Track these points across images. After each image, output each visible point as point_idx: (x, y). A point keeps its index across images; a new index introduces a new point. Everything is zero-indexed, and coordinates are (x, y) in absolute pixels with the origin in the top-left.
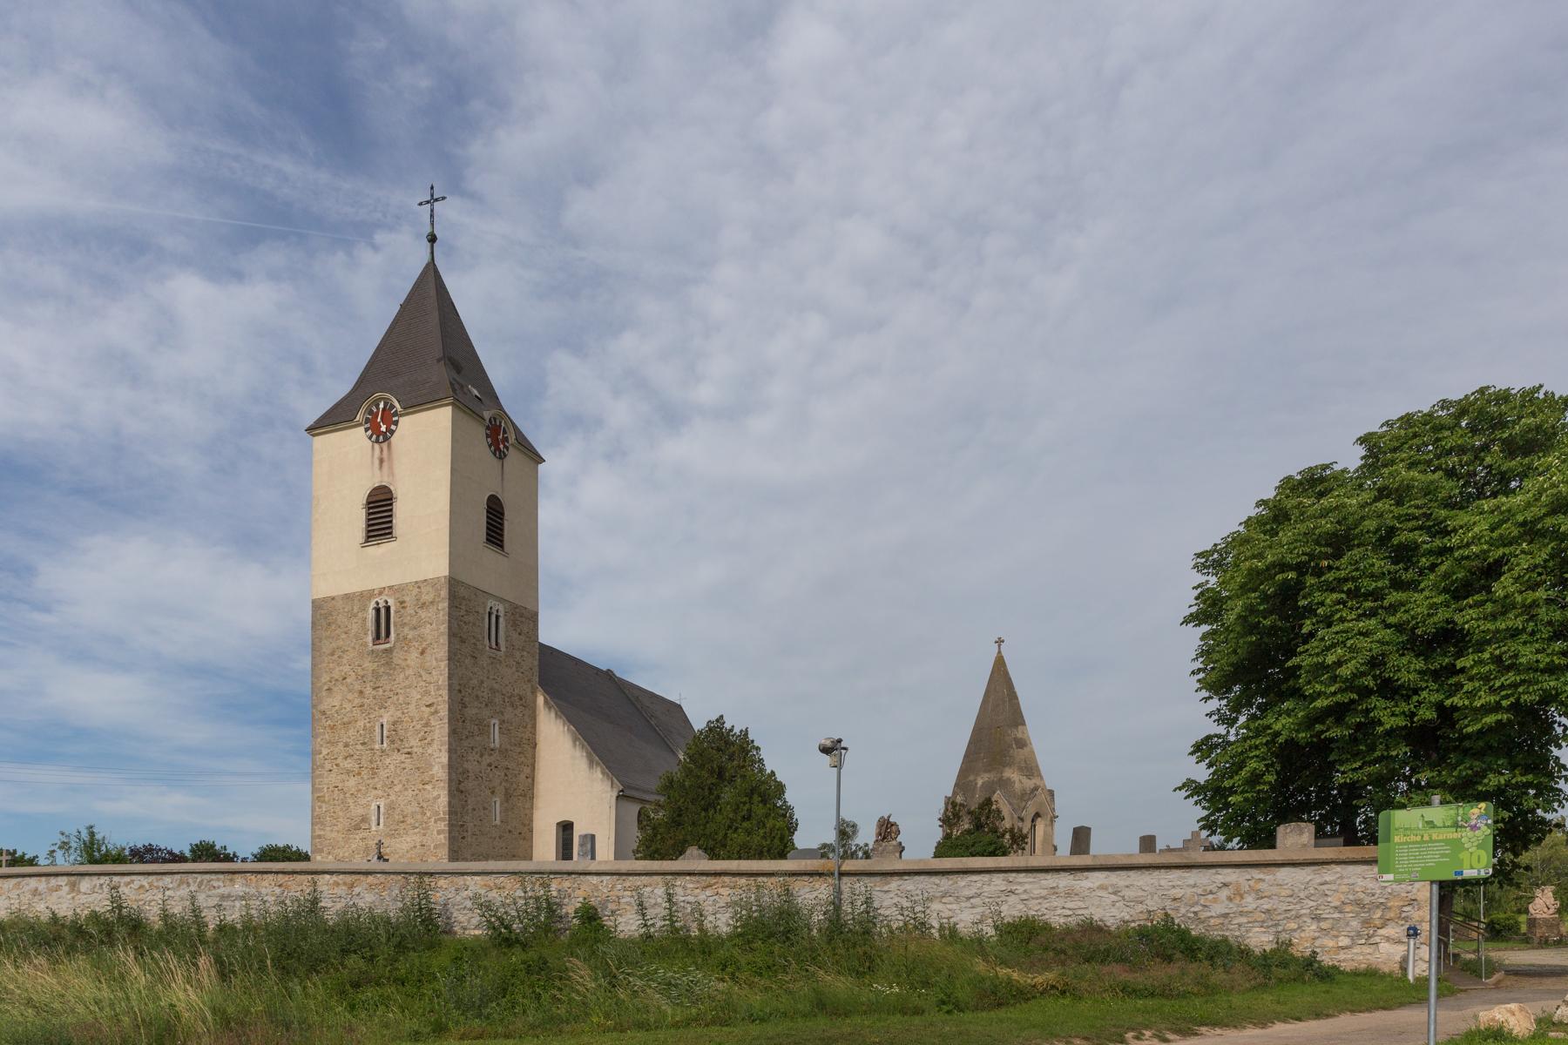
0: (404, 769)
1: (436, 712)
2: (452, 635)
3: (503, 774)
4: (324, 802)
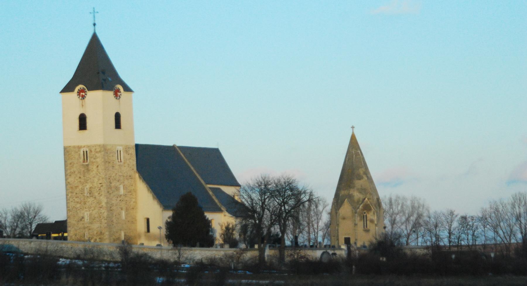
0: (94, 203)
1: (102, 186)
3: (125, 203)
4: (70, 211)
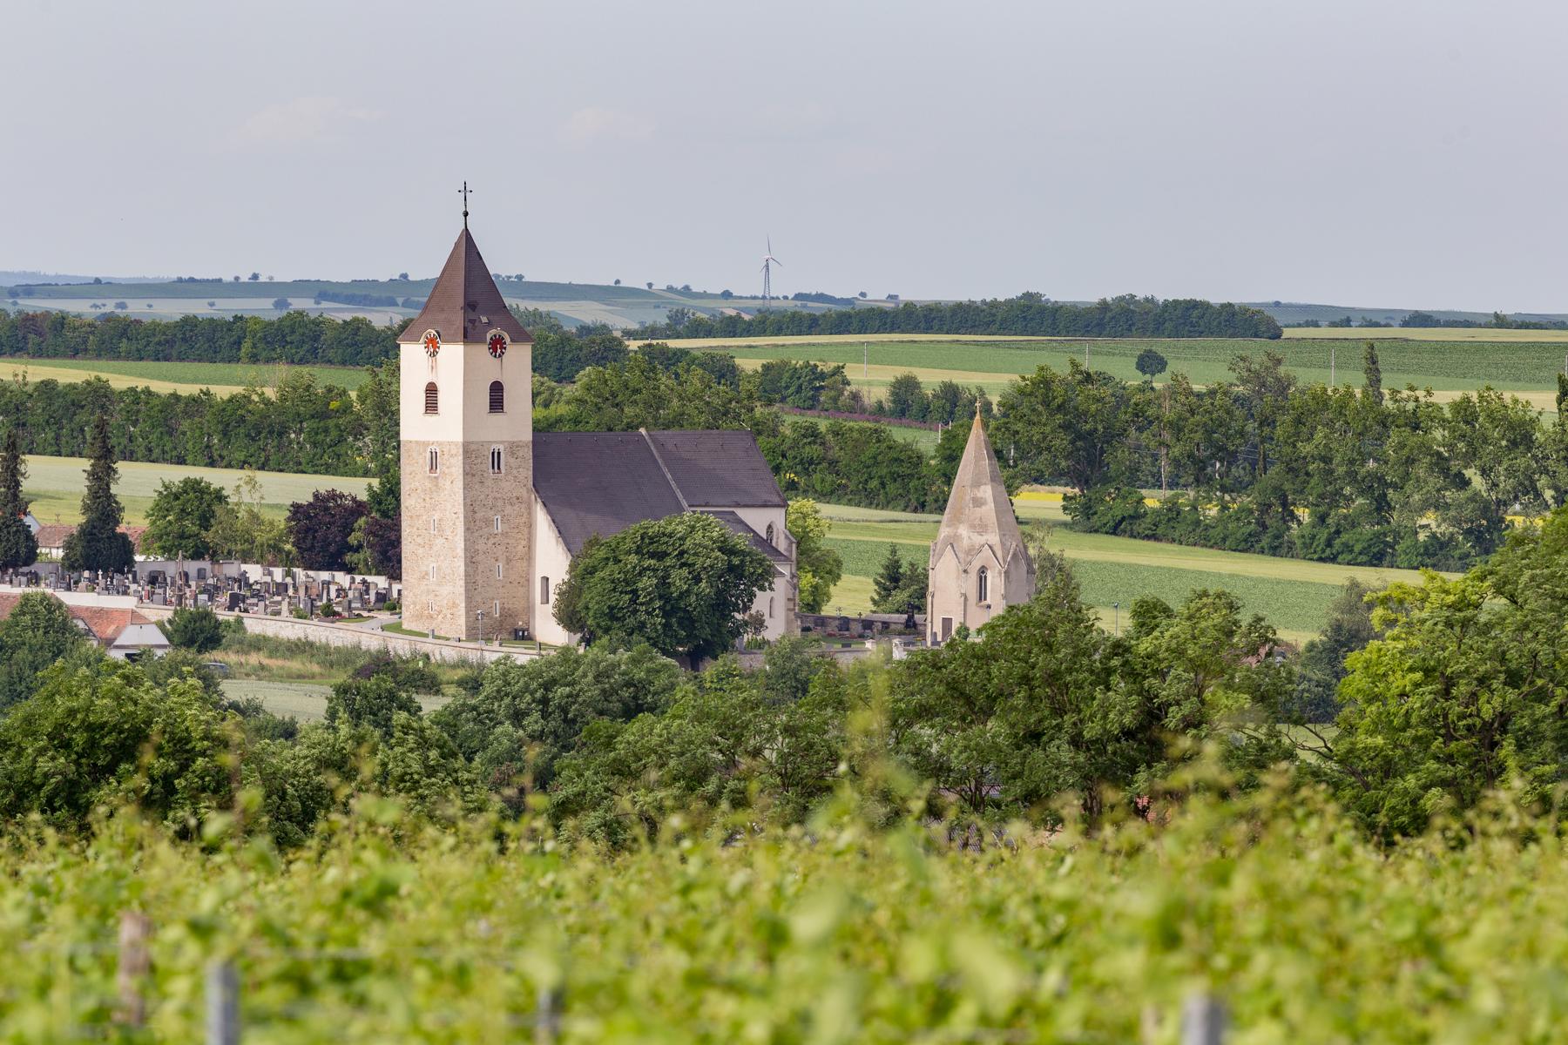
2: (466, 474)
